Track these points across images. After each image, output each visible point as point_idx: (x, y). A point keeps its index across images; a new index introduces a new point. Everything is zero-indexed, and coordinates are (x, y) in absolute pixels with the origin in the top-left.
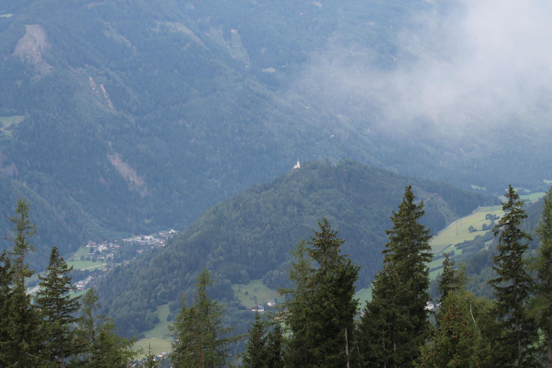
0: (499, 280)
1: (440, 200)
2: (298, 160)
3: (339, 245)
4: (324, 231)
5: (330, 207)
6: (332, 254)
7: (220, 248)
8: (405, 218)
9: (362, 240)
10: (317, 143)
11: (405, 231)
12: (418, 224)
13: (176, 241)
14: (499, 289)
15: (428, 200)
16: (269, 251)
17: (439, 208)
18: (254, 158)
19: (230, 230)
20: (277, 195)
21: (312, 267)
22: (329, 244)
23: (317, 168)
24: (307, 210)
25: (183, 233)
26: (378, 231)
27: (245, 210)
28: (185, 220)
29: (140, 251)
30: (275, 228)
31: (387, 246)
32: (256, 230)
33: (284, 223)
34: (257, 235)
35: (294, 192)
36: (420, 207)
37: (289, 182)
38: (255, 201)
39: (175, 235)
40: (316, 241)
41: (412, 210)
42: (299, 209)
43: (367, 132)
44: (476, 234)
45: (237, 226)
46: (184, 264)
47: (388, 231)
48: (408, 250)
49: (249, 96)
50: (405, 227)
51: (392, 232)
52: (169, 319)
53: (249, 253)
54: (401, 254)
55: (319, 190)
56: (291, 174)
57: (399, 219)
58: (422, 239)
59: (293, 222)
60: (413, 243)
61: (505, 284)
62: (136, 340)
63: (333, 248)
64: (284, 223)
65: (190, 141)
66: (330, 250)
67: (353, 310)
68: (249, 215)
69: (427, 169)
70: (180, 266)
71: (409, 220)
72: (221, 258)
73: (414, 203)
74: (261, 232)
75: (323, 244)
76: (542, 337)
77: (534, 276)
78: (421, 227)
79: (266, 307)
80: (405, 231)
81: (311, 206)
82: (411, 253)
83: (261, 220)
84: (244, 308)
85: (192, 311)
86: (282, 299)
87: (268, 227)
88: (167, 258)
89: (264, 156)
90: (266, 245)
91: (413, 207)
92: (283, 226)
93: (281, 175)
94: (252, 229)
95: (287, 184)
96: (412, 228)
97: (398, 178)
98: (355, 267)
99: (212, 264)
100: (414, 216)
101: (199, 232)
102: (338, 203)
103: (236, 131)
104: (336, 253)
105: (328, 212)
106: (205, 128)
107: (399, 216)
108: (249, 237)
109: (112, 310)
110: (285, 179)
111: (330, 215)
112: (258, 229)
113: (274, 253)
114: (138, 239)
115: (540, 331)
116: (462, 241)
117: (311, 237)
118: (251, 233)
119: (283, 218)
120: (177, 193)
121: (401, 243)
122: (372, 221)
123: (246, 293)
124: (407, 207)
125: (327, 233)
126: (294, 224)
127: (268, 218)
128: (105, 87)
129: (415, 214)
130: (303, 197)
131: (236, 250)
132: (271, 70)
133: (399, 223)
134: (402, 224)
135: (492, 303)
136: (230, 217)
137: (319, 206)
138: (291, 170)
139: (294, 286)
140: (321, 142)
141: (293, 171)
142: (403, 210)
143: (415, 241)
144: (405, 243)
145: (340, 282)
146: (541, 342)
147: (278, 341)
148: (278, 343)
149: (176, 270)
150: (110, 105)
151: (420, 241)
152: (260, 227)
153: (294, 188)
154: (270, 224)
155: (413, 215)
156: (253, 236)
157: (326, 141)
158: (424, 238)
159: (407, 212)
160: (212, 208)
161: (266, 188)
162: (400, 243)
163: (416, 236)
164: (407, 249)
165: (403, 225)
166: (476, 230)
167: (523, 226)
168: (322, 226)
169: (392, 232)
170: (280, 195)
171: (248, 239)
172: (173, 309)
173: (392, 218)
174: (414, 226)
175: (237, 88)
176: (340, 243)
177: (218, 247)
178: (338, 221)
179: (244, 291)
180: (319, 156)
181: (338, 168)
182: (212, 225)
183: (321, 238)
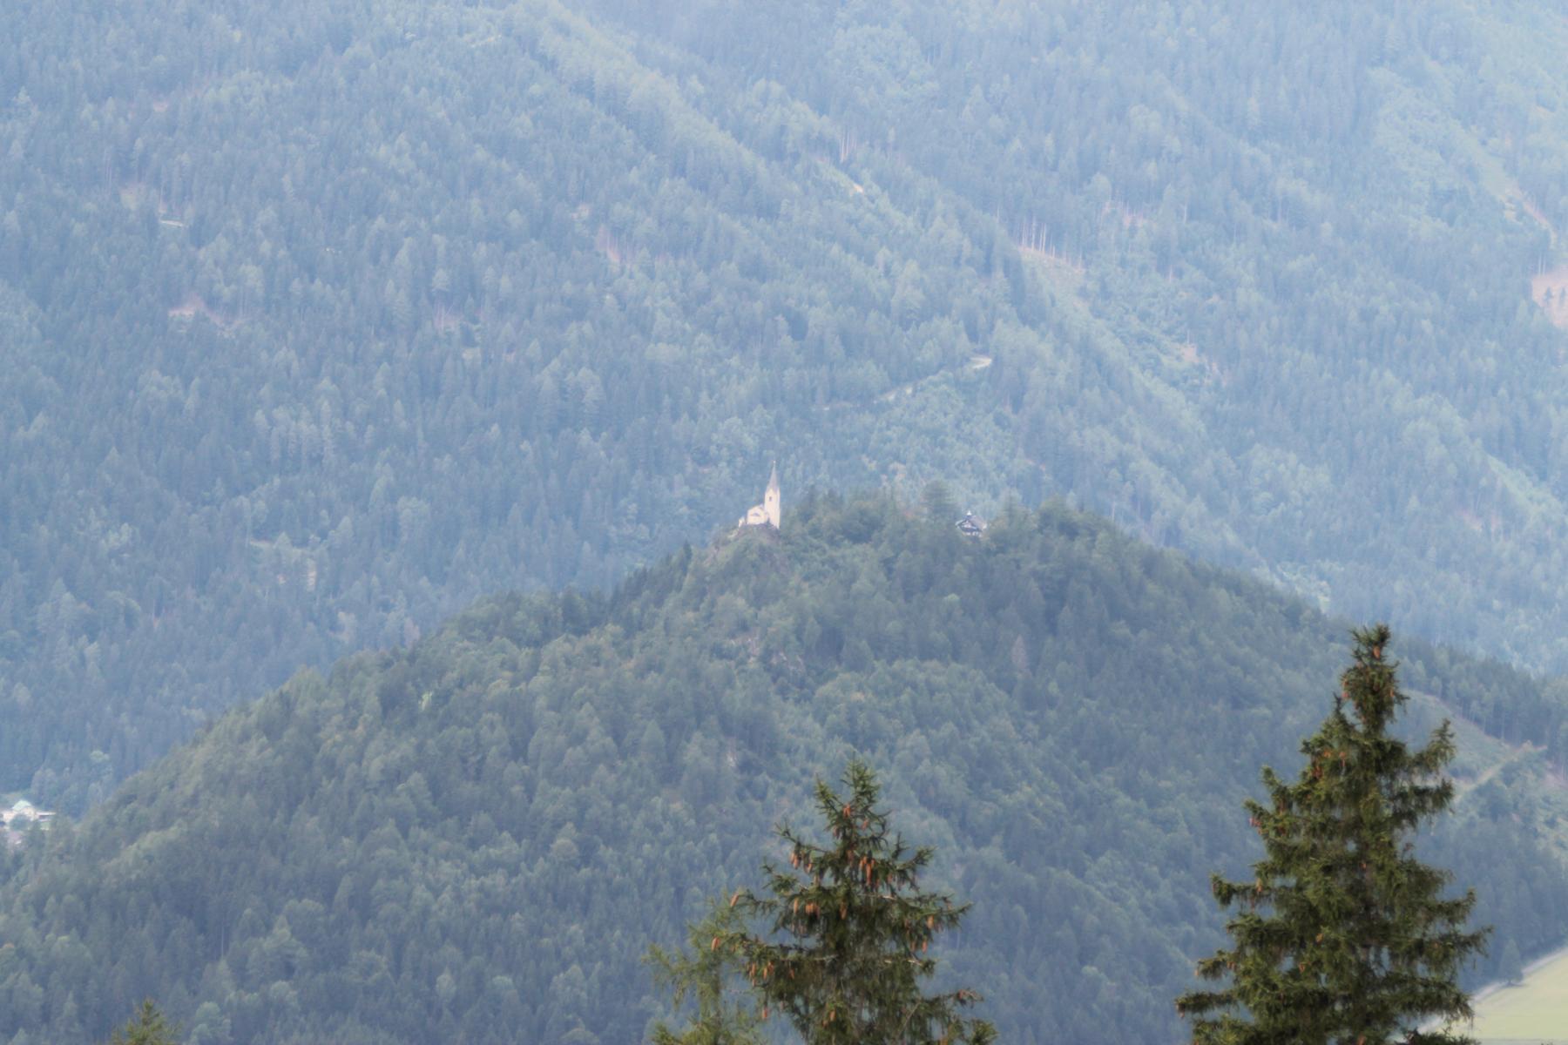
2: (774, 476)
3: (927, 932)
4: (850, 843)
5: (926, 761)
6: (883, 983)
7: (282, 932)
8: (1337, 814)
9: (1090, 970)
10: (891, 397)
11: (1328, 892)
12: (1407, 857)
13: (36, 868)
15: (1484, 779)
16: (555, 978)
17: (1547, 829)
18: (525, 446)
19: (347, 836)
20: (632, 664)
22: (873, 918)
23: (875, 535)
24: (796, 770)
25: (78, 828)
26: (1187, 927)
27: (446, 732)
28: (98, 755)
30: (607, 853)
31: (1213, 969)
32: (494, 852)
33: (657, 829)
34: (498, 880)
35: (730, 658)
37: (708, 598)
38: (505, 688)
39: (35, 838)
40: (792, 898)
41: (1379, 771)
42: (750, 754)
43: (1179, 358)
45: (391, 821)
46: (70, 1006)
47: (1229, 886)
48: (1333, 1002)
49: (535, 89)
50: (1328, 870)
51: (1249, 893)
53: (445, 981)
54: (1291, 1022)
55: (877, 658)
56: (724, 555)
57: (1300, 822)
58: (1420, 947)
59: (711, 826)
60: (1364, 968)
63: (890, 947)
64: (657, 829)
65: (171, 313)
66: (873, 955)
68: (464, 761)
69: (1496, 604)
70: (46, 1015)
71: (1357, 824)
72: (280, 987)
73: (1392, 731)
74: (523, 865)
75: (835, 919)
78: (1424, 881)
80: (1328, 892)
81: (820, 748)
82: (1350, 1024)
83: (531, 801)
87: (564, 841)
89: (585, 437)
90: (545, 940)
91: (1387, 757)
92: (652, 843)
93: (669, 558)
94: (473, 845)
95: (696, 609)
96: (1367, 876)
97: (1331, 638)
99: (228, 1021)
100: (1388, 812)
101: (173, 833)
102: (972, 746)
103: (441, 278)
104: (908, 979)
105: (912, 794)
106: (265, 247)
107: (1300, 802)
108: (449, 887)
110: (688, 580)
111: (923, 810)
112: (508, 847)
113: (584, 995)
117: (770, 870)
118: (465, 865)
119: (658, 802)
120: (68, 596)
121: (1298, 958)
122: (1155, 869)
124: (1353, 754)
125: (863, 854)
126: (713, 837)
127: (568, 790)
129: (1393, 799)
130: (783, 692)
131: (373, 953)
133: (1299, 840)
134: (1314, 851)
136: (354, 765)
137: (868, 753)
138: (727, 531)
140: (915, 391)
141: (736, 540)
142: (1327, 768)
143: (1377, 956)
144: (1318, 963)
149: (21, 1031)
151: (1411, 959)
152: (518, 838)
153: (733, 636)
154: (578, 827)
155: (1383, 801)
156: (474, 883)
157: (944, 387)
158: (1431, 942)
159: (1350, 782)
160: (257, 704)
161: (575, 619)
162: (1288, 963)
163: (1386, 927)
164: (1324, 999)
165: (1318, 857)
168: (839, 809)
169: (1249, 893)
170: (651, 666)
171: (446, 896)
173: (1258, 812)
174: (1381, 868)
175: (467, 37)
176: (938, 918)
177: (269, 927)
178: (963, 848)
180: (895, 472)
181: (994, 547)
182: (248, 797)
183: (828, 880)
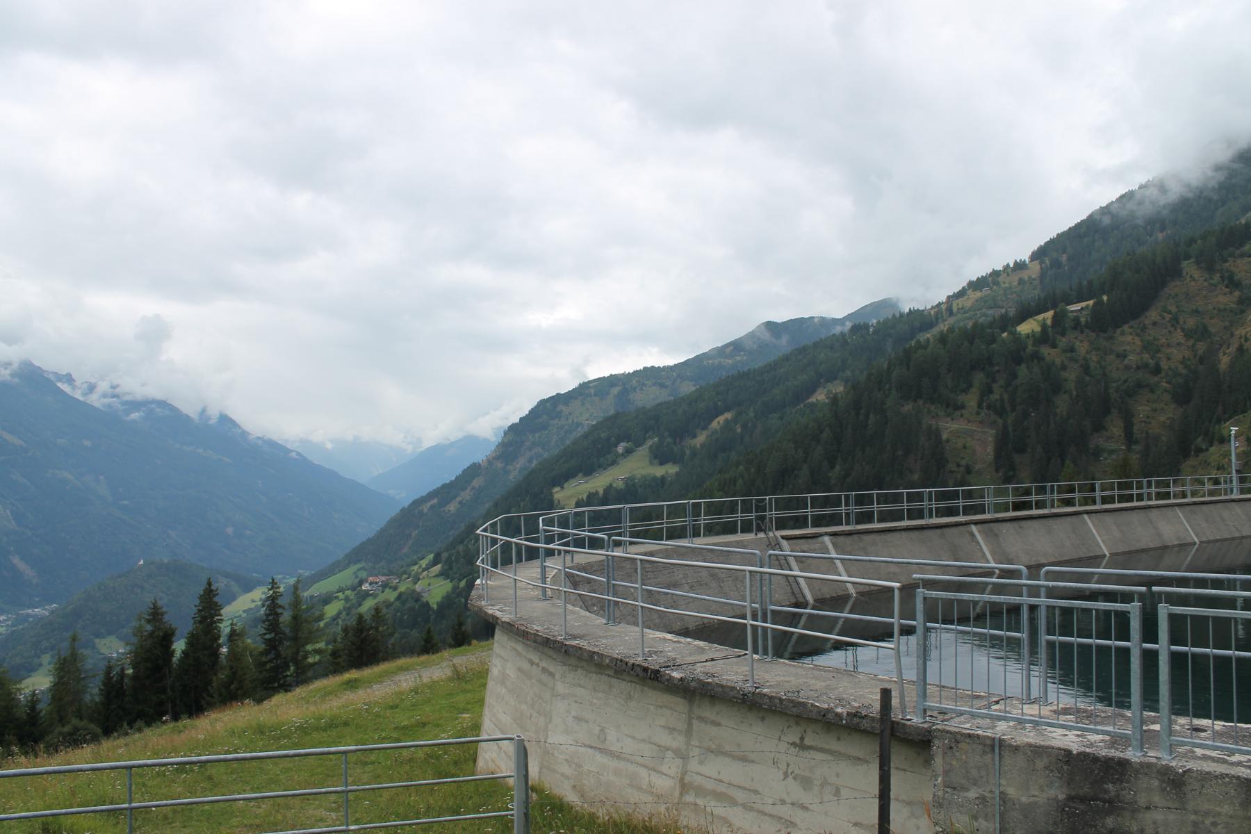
0: (265, 634)
1: (233, 583)
14: (265, 639)
21: (147, 629)
29: (31, 619)
31: (195, 614)
36: (216, 591)
44: (256, 603)
52: (49, 664)
61: (268, 637)
62: (24, 679)
67: (172, 653)
76: (292, 668)
77: (287, 631)
78: (217, 603)
79: (118, 653)
84: (102, 654)
85: (65, 659)
86: (128, 648)
91: (212, 591)
98: (26, 685)
109: (8, 660)
114: (30, 611)
115: (291, 664)
116: (246, 608)
123: (105, 644)
128: (10, 511)
132: (125, 502)
135: (262, 647)
139: (135, 640)
146: (291, 671)
147: (122, 674)
148: (122, 679)
150: (13, 522)
166: (255, 601)
167: (280, 601)
172: (52, 657)
179: (103, 643)
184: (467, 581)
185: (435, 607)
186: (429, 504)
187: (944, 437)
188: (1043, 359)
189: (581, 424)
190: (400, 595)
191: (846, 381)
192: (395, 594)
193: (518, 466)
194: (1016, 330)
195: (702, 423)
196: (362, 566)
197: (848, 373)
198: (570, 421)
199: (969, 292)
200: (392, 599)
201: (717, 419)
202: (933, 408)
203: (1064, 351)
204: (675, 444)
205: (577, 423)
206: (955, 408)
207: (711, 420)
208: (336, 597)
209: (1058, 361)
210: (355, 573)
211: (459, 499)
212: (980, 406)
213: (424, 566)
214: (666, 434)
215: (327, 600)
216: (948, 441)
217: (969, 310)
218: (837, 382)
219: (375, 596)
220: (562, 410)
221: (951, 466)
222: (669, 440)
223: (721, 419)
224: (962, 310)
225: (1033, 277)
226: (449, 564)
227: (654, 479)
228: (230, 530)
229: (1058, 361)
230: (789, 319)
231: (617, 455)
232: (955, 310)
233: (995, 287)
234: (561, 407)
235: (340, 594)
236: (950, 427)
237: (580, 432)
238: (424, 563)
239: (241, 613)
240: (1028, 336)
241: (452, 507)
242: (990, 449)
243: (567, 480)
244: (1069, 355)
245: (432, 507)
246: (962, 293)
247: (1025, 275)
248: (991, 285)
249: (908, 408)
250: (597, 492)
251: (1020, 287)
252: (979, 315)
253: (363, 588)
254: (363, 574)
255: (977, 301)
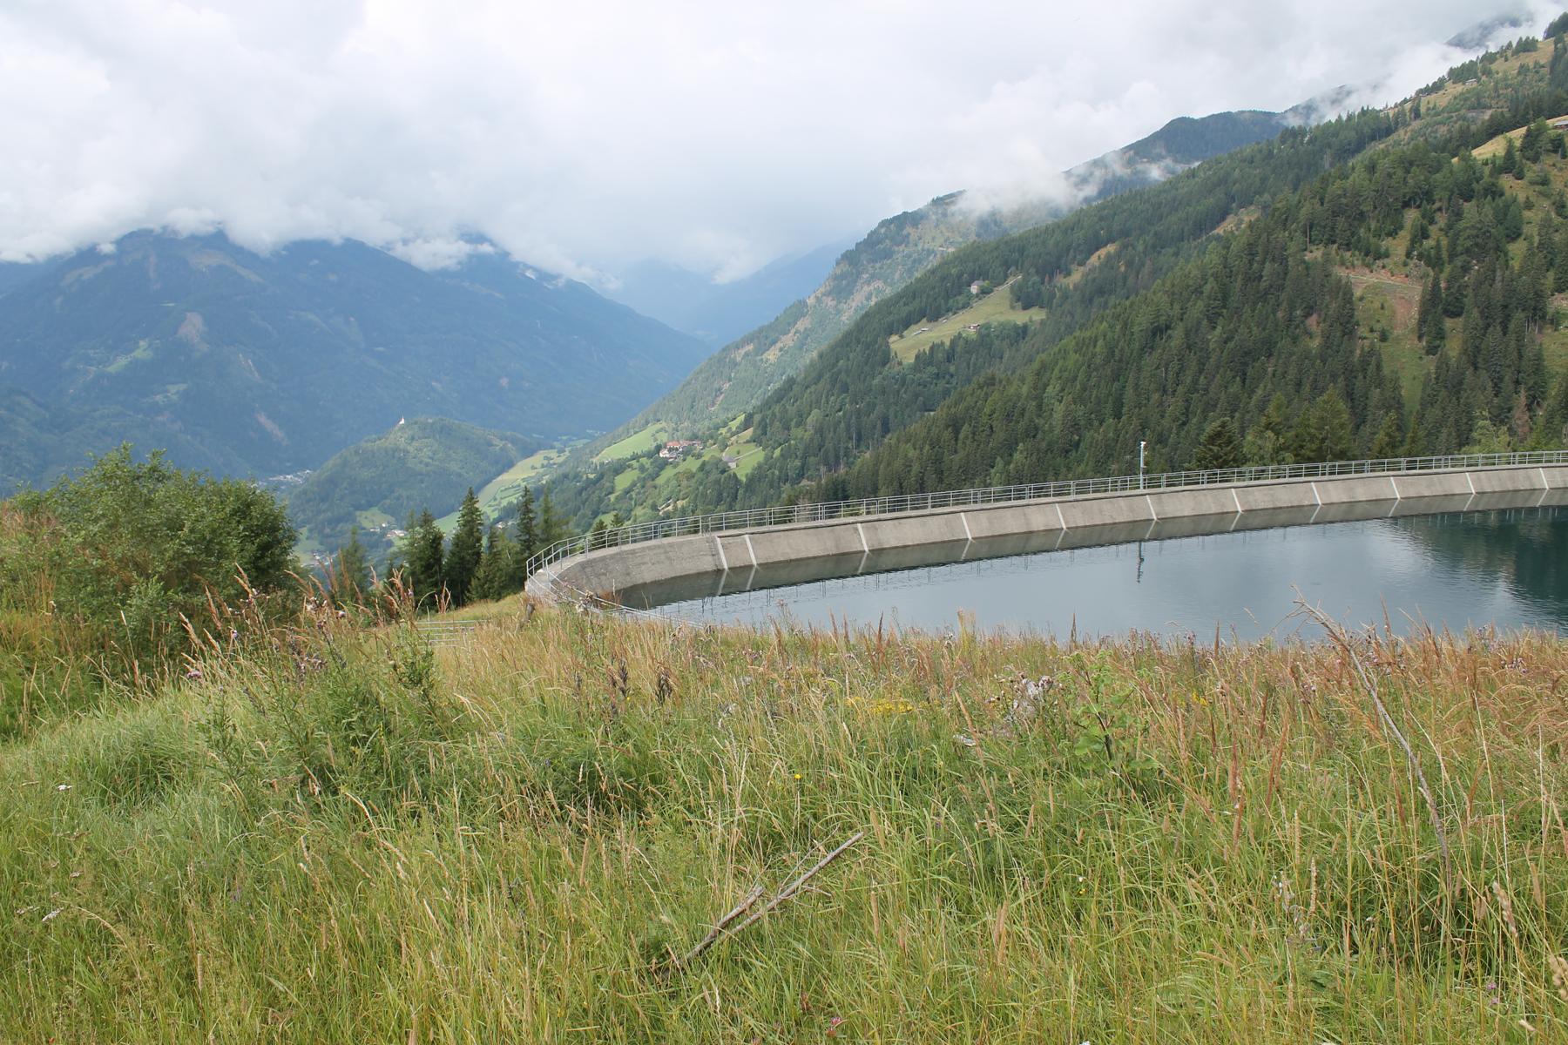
61: (523, 538)
84: (364, 529)
88: (305, 492)
114: (281, 478)
132: (381, 349)
135: (518, 548)
145: (434, 541)
150: (256, 374)
184: (782, 450)
185: (744, 479)
186: (742, 351)
187: (1358, 293)
188: (1502, 194)
189: (933, 251)
190: (704, 464)
191: (1265, 208)
192: (698, 463)
193: (854, 304)
194: (1470, 155)
195: (1079, 257)
196: (661, 426)
197: (1267, 197)
198: (920, 248)
199: (1449, 85)
200: (694, 470)
201: (1098, 253)
202: (1348, 254)
203: (1533, 183)
204: (1043, 283)
205: (928, 250)
206: (1374, 255)
207: (1091, 253)
208: (629, 466)
209: (1521, 198)
210: (653, 435)
211: (779, 345)
212: (1408, 255)
213: (734, 429)
214: (1032, 270)
215: (619, 468)
216: (1361, 299)
217: (1443, 111)
218: (1252, 208)
219: (675, 465)
220: (909, 234)
221: (1362, 331)
222: (1036, 278)
223: (1103, 252)
224: (1434, 111)
225: (1542, 62)
226: (764, 428)
227: (1016, 327)
228: (504, 382)
229: (1521, 198)
230: (1210, 114)
231: (970, 296)
232: (1423, 110)
233: (1484, 78)
234: (908, 230)
235: (634, 462)
236: (1363, 279)
237: (933, 262)
238: (734, 425)
239: (519, 481)
240: (1486, 163)
241: (772, 355)
242: (1415, 312)
243: (907, 326)
244: (1538, 188)
245: (747, 354)
246: (1437, 87)
247: (1529, 59)
248: (1480, 74)
249: (1315, 254)
250: (942, 343)
251: (1520, 78)
252: (1455, 118)
253: (661, 455)
254: (663, 437)
255: (1455, 98)
